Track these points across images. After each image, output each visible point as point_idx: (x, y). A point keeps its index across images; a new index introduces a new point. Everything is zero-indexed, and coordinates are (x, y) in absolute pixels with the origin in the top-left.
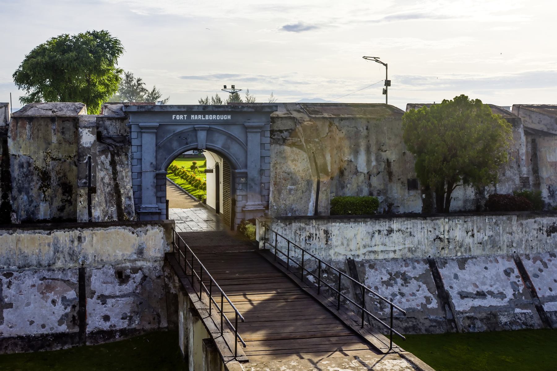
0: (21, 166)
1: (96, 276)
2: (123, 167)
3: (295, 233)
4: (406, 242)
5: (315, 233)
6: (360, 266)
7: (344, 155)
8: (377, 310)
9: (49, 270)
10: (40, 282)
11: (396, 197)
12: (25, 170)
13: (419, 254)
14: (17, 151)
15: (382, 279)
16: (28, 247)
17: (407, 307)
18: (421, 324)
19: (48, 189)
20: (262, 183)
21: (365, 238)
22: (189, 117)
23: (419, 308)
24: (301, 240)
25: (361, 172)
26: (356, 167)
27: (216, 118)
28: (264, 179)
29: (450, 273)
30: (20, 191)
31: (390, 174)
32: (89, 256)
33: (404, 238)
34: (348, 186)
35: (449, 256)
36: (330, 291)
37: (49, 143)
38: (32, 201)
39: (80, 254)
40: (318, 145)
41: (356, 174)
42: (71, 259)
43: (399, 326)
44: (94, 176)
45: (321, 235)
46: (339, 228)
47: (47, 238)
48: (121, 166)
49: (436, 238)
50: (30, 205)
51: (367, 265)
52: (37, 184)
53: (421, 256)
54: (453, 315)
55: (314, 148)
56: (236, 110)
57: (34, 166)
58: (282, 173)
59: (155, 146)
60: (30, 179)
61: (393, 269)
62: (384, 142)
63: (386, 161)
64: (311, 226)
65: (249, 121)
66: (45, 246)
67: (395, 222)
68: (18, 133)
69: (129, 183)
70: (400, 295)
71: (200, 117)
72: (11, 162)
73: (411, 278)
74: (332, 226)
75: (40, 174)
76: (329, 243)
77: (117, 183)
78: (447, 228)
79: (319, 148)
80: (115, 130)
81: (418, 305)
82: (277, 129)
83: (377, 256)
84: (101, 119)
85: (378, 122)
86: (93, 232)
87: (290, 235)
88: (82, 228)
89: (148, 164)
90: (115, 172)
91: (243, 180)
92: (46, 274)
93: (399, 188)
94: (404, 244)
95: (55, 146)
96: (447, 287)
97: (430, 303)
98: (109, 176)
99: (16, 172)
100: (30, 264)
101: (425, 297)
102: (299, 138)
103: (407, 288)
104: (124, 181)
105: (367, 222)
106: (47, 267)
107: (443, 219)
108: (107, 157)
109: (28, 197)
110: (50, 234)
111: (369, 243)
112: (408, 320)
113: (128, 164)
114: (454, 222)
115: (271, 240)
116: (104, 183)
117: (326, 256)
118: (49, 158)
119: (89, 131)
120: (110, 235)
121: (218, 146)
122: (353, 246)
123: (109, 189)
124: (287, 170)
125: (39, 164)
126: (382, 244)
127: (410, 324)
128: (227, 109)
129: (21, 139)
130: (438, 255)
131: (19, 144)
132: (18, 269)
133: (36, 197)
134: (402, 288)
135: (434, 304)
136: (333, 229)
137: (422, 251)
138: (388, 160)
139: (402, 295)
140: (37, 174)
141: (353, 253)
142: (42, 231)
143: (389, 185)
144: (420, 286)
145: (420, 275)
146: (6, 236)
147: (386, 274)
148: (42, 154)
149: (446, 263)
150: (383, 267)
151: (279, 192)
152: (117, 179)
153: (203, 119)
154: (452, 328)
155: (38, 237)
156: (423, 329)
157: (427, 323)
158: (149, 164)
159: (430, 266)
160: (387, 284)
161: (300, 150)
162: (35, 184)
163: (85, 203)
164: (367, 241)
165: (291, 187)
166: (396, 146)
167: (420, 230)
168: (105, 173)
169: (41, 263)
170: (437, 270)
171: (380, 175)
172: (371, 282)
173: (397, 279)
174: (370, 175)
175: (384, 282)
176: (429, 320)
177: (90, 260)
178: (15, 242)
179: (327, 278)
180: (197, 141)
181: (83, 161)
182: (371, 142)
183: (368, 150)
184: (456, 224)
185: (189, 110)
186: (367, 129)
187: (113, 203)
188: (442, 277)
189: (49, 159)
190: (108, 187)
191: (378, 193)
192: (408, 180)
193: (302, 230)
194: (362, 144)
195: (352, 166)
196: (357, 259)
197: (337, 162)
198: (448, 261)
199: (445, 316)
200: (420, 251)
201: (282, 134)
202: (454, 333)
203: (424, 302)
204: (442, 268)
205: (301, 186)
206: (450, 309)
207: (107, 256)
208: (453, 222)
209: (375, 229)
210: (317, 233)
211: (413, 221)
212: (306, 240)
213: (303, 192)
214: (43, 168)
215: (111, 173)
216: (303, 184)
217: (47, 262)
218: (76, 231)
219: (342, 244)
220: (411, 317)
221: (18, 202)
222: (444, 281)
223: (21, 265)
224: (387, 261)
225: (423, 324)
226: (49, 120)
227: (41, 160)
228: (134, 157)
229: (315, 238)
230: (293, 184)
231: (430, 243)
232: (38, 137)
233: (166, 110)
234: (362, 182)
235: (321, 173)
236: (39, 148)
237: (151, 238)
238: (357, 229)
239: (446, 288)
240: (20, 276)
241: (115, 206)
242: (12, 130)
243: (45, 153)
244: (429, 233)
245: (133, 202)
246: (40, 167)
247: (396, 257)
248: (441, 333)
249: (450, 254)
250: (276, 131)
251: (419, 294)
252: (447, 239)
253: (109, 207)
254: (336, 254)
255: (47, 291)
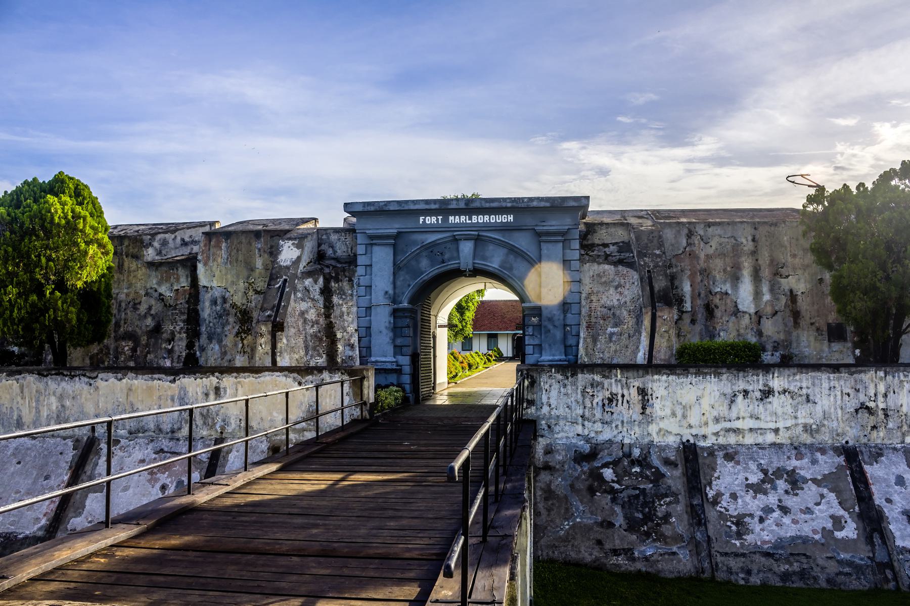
0: (214, 302)
1: (238, 451)
2: (344, 299)
3: (584, 392)
4: (799, 414)
5: (620, 392)
6: (706, 455)
7: (714, 284)
8: (731, 537)
9: (171, 439)
10: (154, 456)
11: (807, 354)
12: (218, 308)
13: (825, 438)
14: (209, 281)
15: (747, 479)
16: (142, 401)
17: (793, 534)
18: (819, 569)
19: (248, 335)
20: (565, 325)
21: (716, 406)
22: (446, 220)
23: (817, 537)
24: (595, 404)
25: (744, 312)
26: (736, 302)
27: (489, 219)
28: (571, 319)
29: (887, 474)
30: (210, 339)
31: (796, 315)
32: (232, 419)
33: (795, 407)
34: (722, 334)
35: (887, 442)
36: (641, 498)
37: (252, 269)
38: (225, 353)
39: (217, 415)
40: (659, 260)
41: (735, 315)
42: (205, 423)
43: (771, 570)
44: (284, 306)
45: (632, 396)
46: (667, 385)
47: (170, 388)
48: (341, 298)
49: (861, 408)
50: (222, 359)
51: (721, 454)
52: (234, 328)
53: (830, 442)
54: (889, 555)
55: (652, 265)
56: (520, 205)
57: (231, 302)
58: (599, 309)
59: (391, 265)
60: (225, 321)
61: (772, 462)
62: (783, 261)
63: (789, 293)
64: (613, 380)
65: (544, 224)
66: (167, 400)
67: (776, 375)
68: (211, 255)
69: (352, 323)
70: (781, 510)
71: (463, 218)
72: (201, 297)
73: (805, 481)
74: (653, 381)
75: (238, 314)
76: (648, 411)
77: (331, 322)
78: (882, 388)
79: (660, 264)
80: (344, 248)
81: (815, 532)
82: (600, 242)
83: (741, 439)
84: (325, 233)
85: (772, 228)
86: (238, 380)
87: (574, 395)
88: (222, 373)
89: (381, 294)
90: (329, 306)
91: (535, 320)
92: (165, 444)
93: (812, 339)
94: (796, 418)
95: (260, 273)
96: (878, 500)
97: (842, 529)
98: (317, 310)
99: (206, 311)
100: (146, 428)
101: (832, 517)
102: (632, 253)
103: (795, 499)
104: (344, 321)
105: (720, 374)
106: (170, 434)
107: (873, 372)
108: (316, 282)
109: (220, 347)
110: (174, 381)
111: (726, 413)
112: (791, 559)
113: (352, 295)
114: (897, 378)
115: (538, 403)
116: (305, 321)
117: (643, 437)
118: (251, 291)
119: (293, 244)
120: (264, 385)
121: (493, 266)
122: (694, 418)
123: (315, 329)
124: (608, 302)
125: (238, 299)
126: (751, 417)
127: (796, 567)
128: (504, 205)
129: (215, 263)
130: (864, 440)
131: (211, 271)
132: (128, 435)
133: (231, 346)
134: (785, 498)
135: (850, 531)
136: (655, 386)
137: (832, 431)
138: (791, 291)
139: (785, 510)
140: (234, 313)
141: (694, 431)
142: (163, 376)
143: (795, 334)
144: (822, 496)
145: (824, 475)
146: (113, 382)
147: (756, 471)
148: (242, 285)
149: (881, 455)
150: (751, 459)
151: (595, 340)
152: (332, 316)
153: (468, 221)
154: (887, 580)
155: (157, 386)
156: (822, 578)
157: (833, 568)
158: (383, 293)
159: (848, 460)
160: (757, 489)
161: (628, 269)
162: (232, 328)
163: (267, 346)
164: (723, 410)
165: (613, 330)
166: (805, 267)
167: (827, 392)
168: (310, 304)
169: (162, 427)
170: (862, 468)
171: (779, 317)
172: (724, 485)
173: (778, 482)
174: (760, 317)
175: (749, 487)
176: (838, 561)
177: (233, 426)
178: (125, 391)
179: (641, 474)
180: (459, 258)
181: (274, 285)
182: (760, 262)
183: (756, 277)
184: (901, 382)
185: (443, 207)
186: (754, 240)
187: (321, 352)
188: (870, 481)
189: (251, 293)
190: (312, 326)
191: (774, 347)
192: (829, 325)
193: (597, 387)
194: (746, 264)
195: (728, 301)
196: (702, 444)
197: (702, 295)
198: (885, 452)
199: (871, 555)
200: (827, 431)
201: (607, 249)
202: (889, 590)
203: (829, 525)
204: (872, 464)
205: (628, 327)
206: (884, 542)
207: (259, 420)
208: (894, 377)
209: (736, 388)
210: (626, 392)
211: (813, 374)
212: (604, 405)
213: (629, 337)
214: (243, 305)
215: (322, 306)
216: (630, 324)
217: (170, 426)
218: (212, 378)
219: (674, 414)
220: (798, 554)
221: (207, 354)
222: (874, 488)
223: (133, 430)
224: (760, 448)
225: (823, 568)
226: (252, 236)
227: (240, 294)
228: (361, 284)
229: (620, 402)
230: (616, 325)
231: (847, 416)
232: (237, 260)
233: (406, 208)
234: (746, 328)
235: (659, 302)
236: (238, 277)
237: (329, 393)
238: (702, 387)
239: (877, 502)
240: (129, 446)
241: (324, 356)
242: (203, 250)
243: (246, 284)
244: (846, 398)
245: (357, 352)
246: (239, 304)
247: (778, 441)
248: (861, 588)
249: (890, 439)
250: (598, 245)
251: (819, 510)
252: (883, 409)
253: (312, 356)
254: (662, 433)
255: (158, 471)
